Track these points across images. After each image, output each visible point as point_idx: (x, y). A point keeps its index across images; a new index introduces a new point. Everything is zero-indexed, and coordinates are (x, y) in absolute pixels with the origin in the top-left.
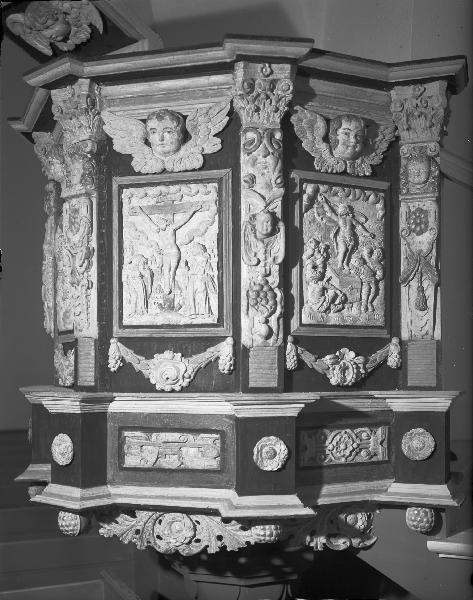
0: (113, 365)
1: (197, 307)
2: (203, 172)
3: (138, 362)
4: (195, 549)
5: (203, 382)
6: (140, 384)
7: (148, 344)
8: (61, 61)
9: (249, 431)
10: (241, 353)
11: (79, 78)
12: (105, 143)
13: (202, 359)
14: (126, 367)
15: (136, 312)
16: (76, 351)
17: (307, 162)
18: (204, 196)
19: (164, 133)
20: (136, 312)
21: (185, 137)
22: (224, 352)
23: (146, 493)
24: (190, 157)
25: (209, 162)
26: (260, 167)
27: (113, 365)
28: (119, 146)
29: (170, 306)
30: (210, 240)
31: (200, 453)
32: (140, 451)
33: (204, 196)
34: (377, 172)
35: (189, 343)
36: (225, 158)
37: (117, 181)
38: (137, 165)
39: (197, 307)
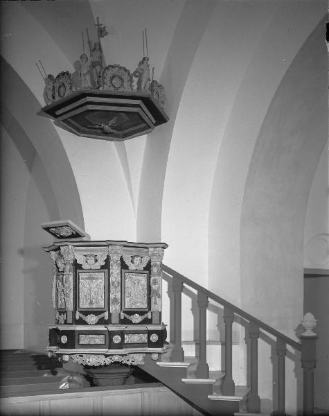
0: (77, 318)
3: (84, 317)
9: (111, 334)
13: (100, 316)
23: (92, 342)
24: (98, 265)
26: (115, 270)
27: (77, 318)
36: (106, 266)
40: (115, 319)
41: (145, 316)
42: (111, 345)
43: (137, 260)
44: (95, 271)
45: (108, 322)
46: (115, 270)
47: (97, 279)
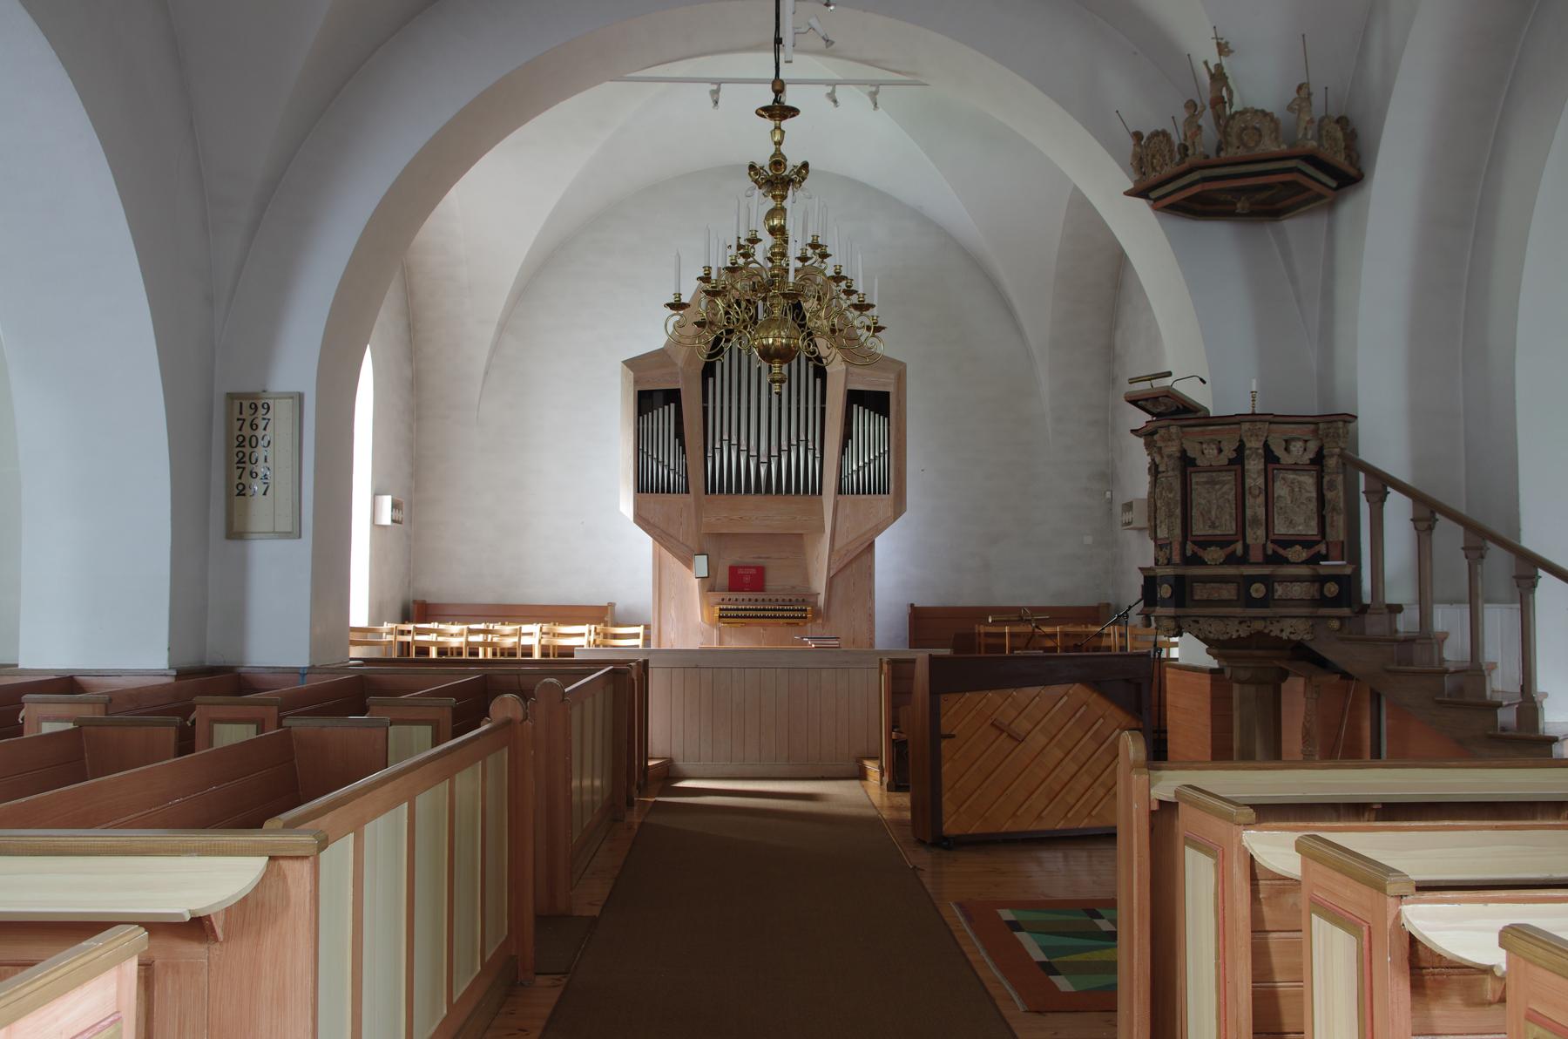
0: (1189, 553)
1: (1228, 527)
2: (1174, 718)
3: (1201, 553)
4: (1226, 637)
5: (1231, 560)
6: (1202, 562)
7: (1204, 543)
8: (1292, 824)
10: (1246, 547)
11: (1168, 411)
12: (1184, 452)
14: (1194, 554)
15: (1199, 529)
16: (409, 293)
17: (1277, 460)
18: (1229, 477)
19: (1211, 451)
20: (1199, 529)
21: (1220, 451)
22: (1239, 547)
23: (1215, 596)
25: (1231, 462)
26: (1254, 466)
28: (1190, 454)
29: (1213, 526)
30: (1231, 496)
31: (1228, 592)
32: (1200, 592)
33: (1229, 477)
34: (1313, 462)
35: (1223, 543)
37: (1190, 469)
38: (1199, 462)
39: (1228, 527)
40: (1256, 555)
41: (1231, 548)
42: (1250, 602)
43: (1296, 447)
44: (1220, 470)
45: (1243, 560)
46: (1254, 466)
47: (1224, 483)
